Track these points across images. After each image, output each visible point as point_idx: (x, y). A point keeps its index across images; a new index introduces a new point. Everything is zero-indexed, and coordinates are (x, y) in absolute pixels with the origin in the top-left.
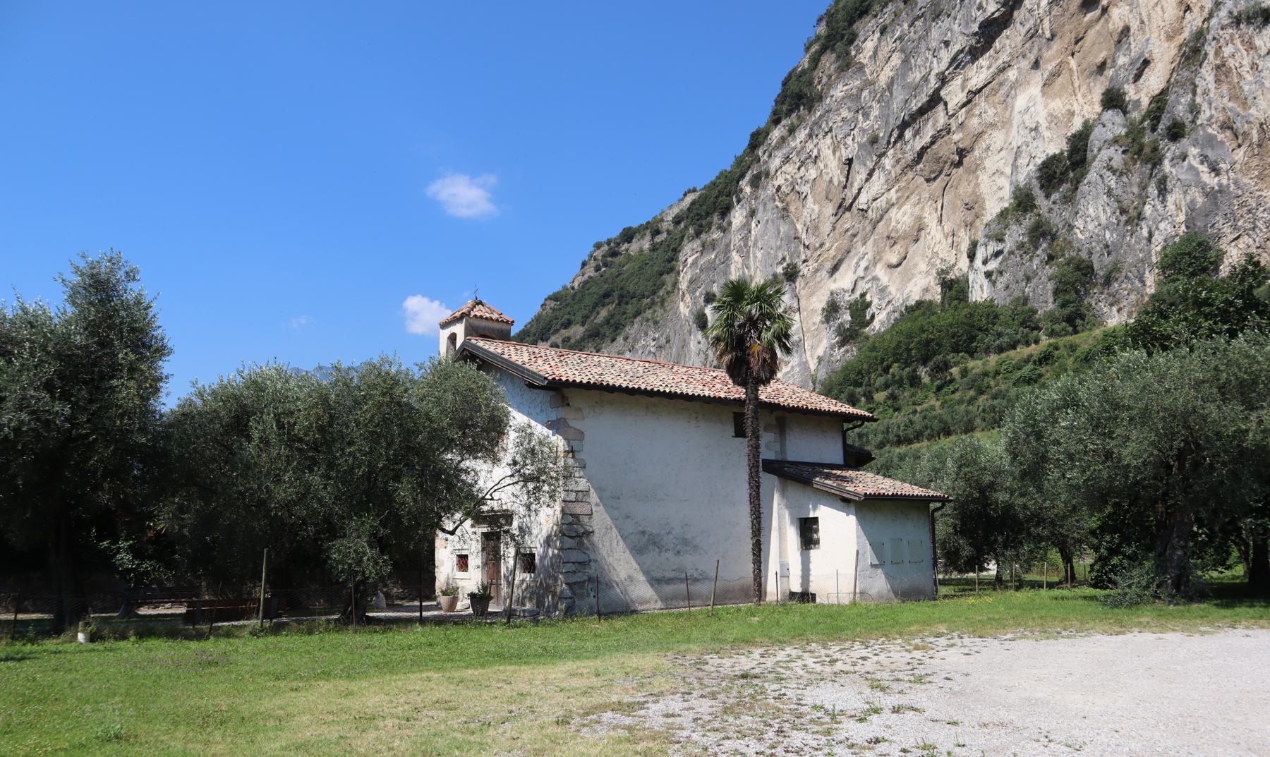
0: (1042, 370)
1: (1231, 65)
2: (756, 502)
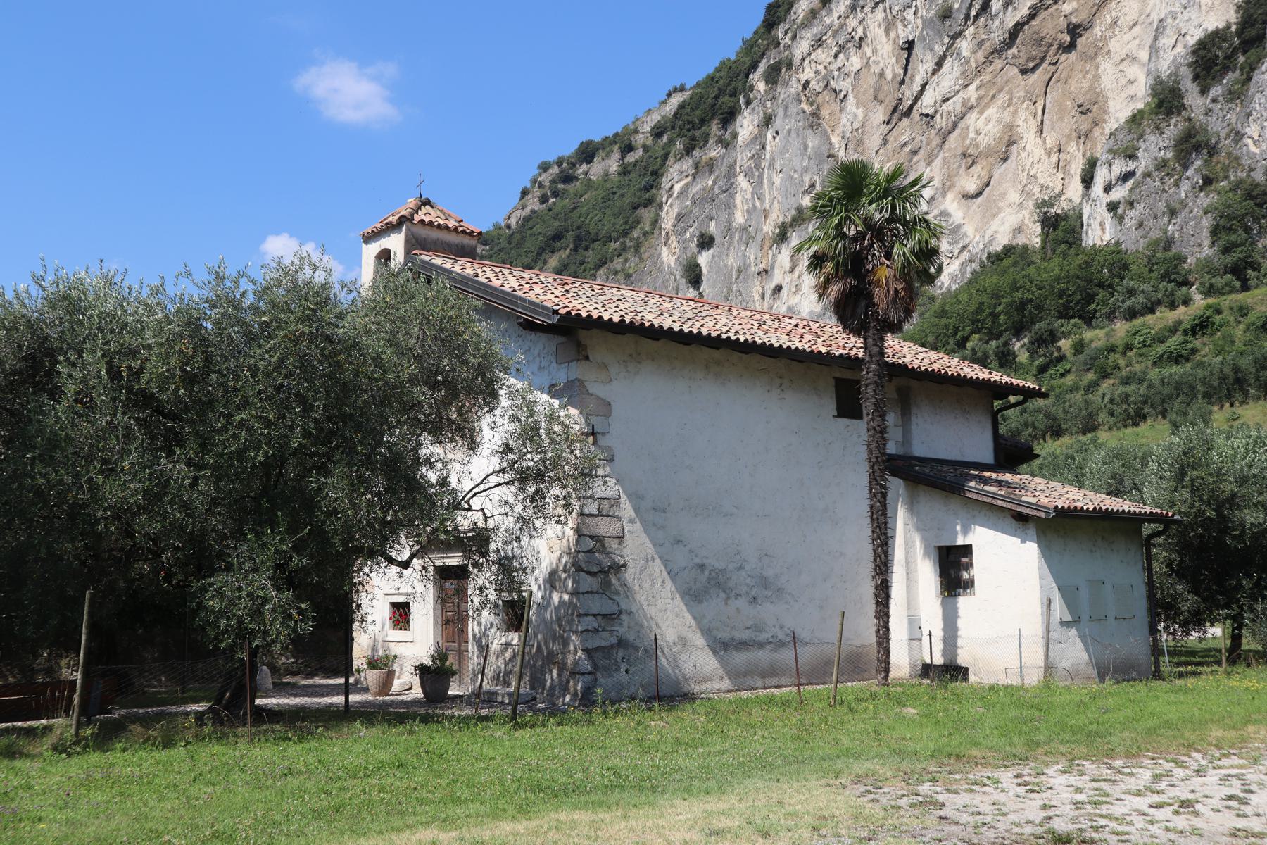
0: (1197, 343)
2: (882, 519)
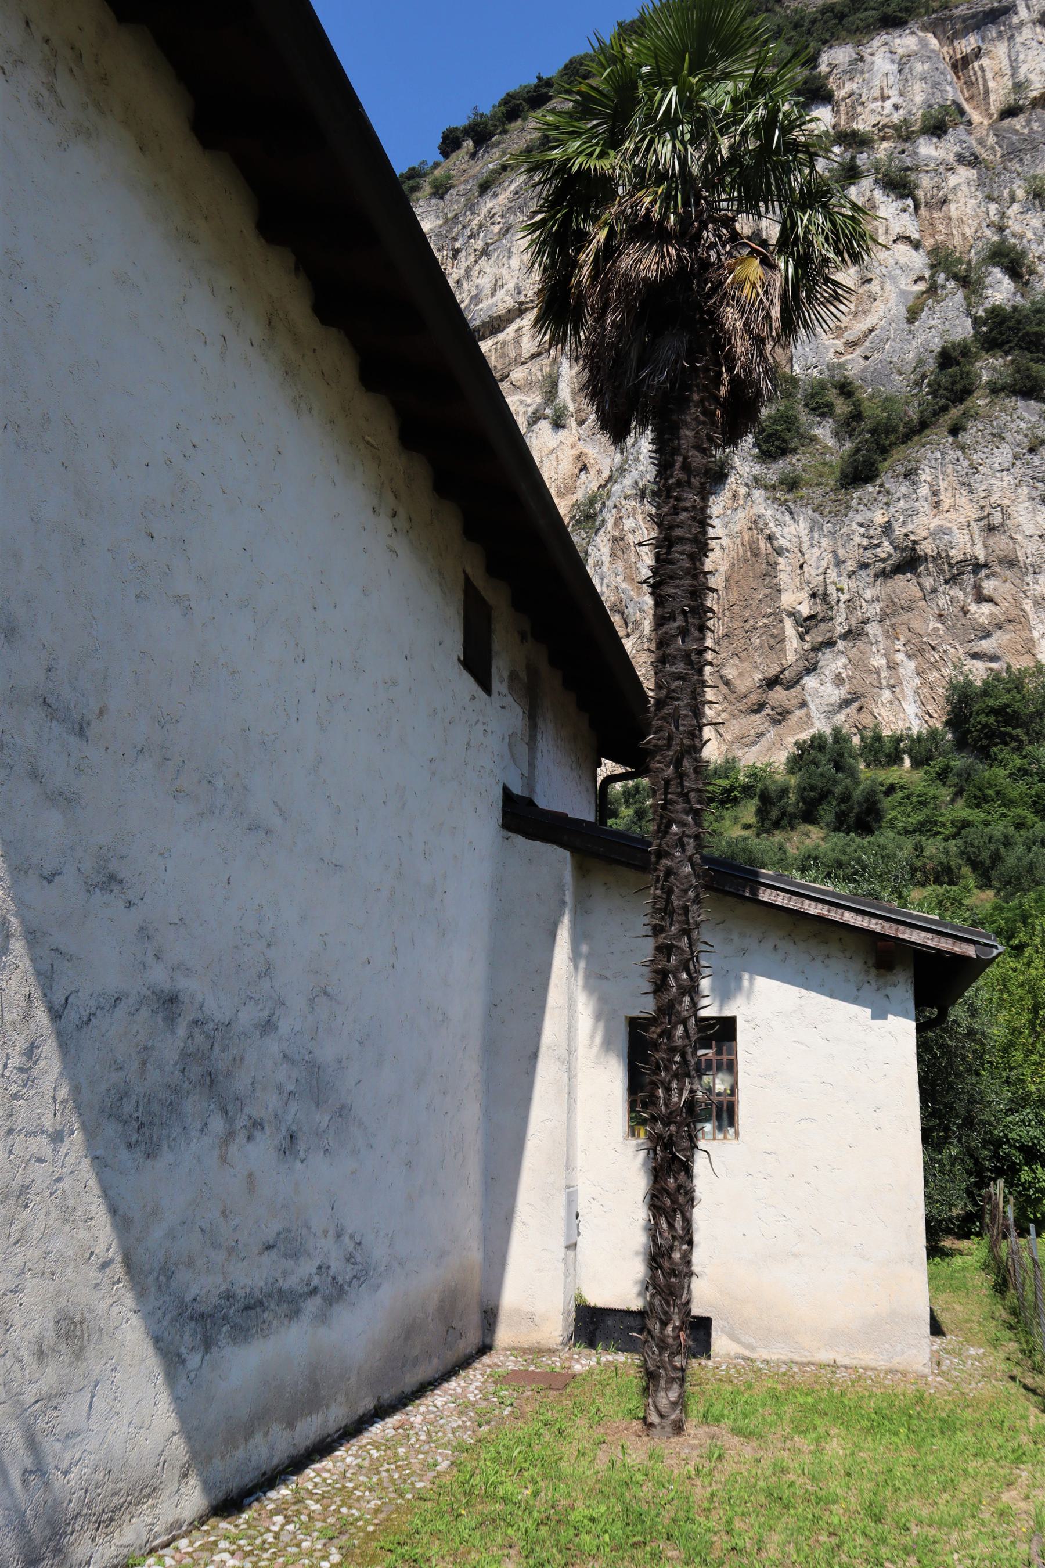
1: (631, 541)
